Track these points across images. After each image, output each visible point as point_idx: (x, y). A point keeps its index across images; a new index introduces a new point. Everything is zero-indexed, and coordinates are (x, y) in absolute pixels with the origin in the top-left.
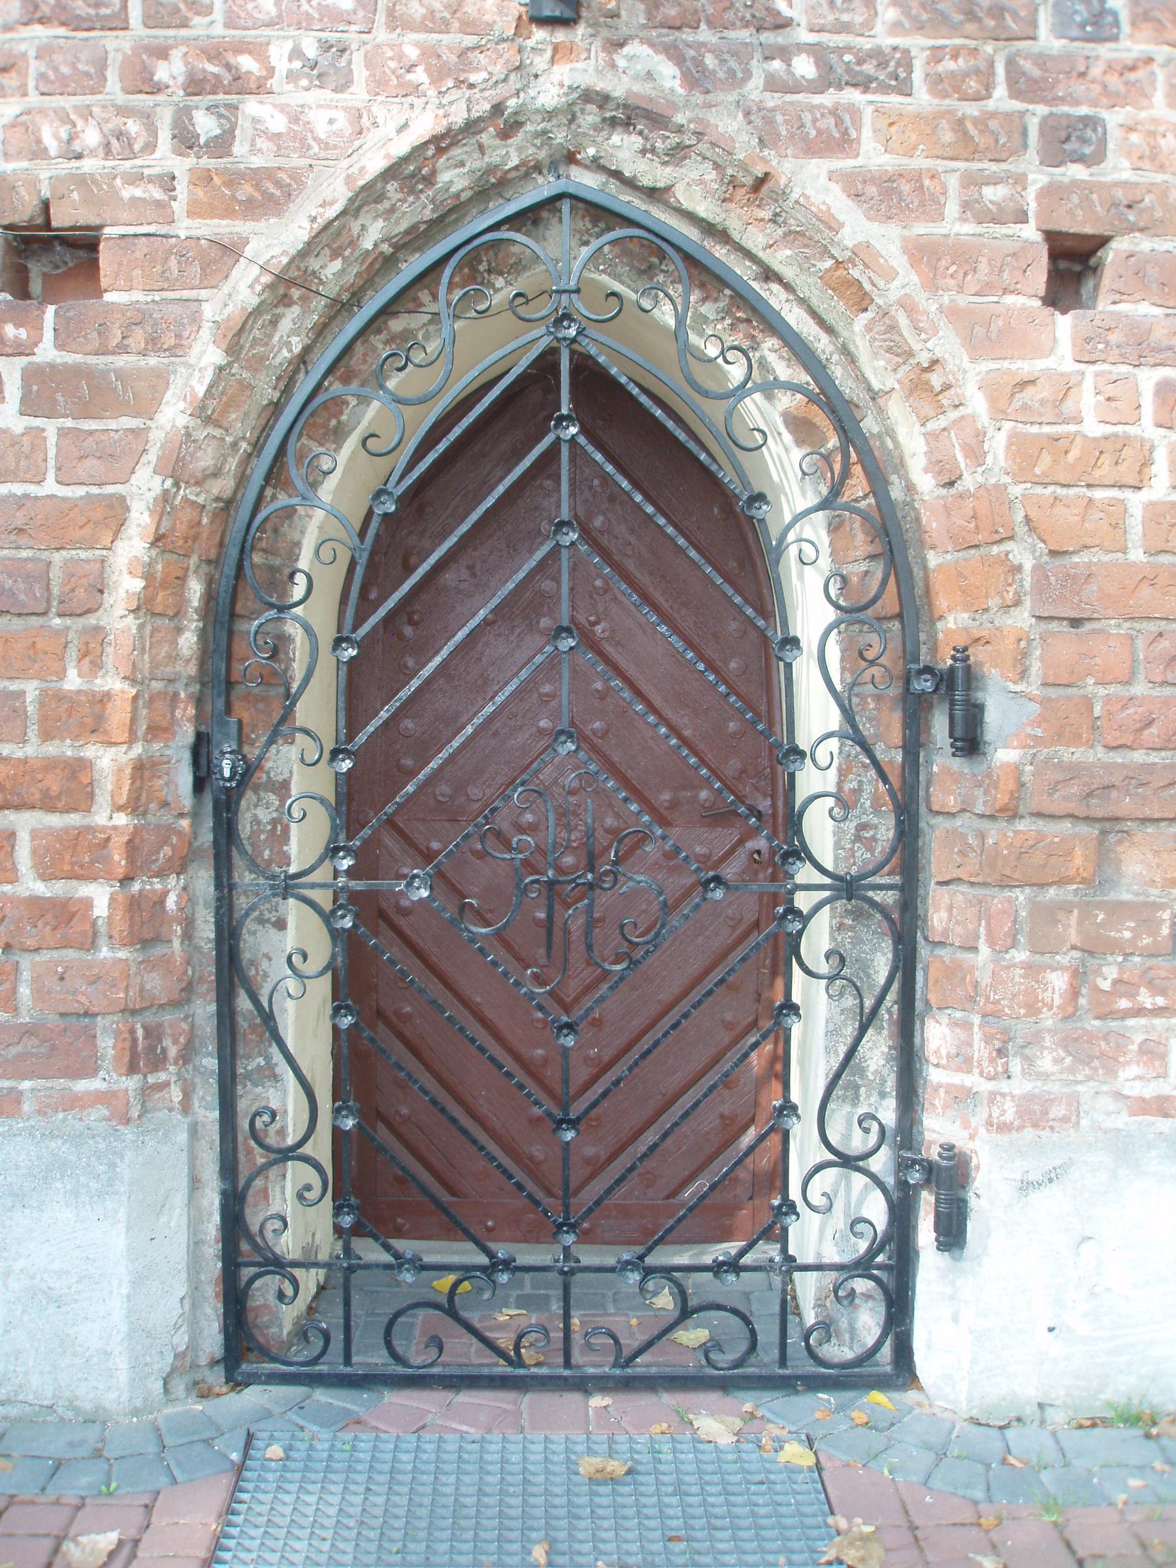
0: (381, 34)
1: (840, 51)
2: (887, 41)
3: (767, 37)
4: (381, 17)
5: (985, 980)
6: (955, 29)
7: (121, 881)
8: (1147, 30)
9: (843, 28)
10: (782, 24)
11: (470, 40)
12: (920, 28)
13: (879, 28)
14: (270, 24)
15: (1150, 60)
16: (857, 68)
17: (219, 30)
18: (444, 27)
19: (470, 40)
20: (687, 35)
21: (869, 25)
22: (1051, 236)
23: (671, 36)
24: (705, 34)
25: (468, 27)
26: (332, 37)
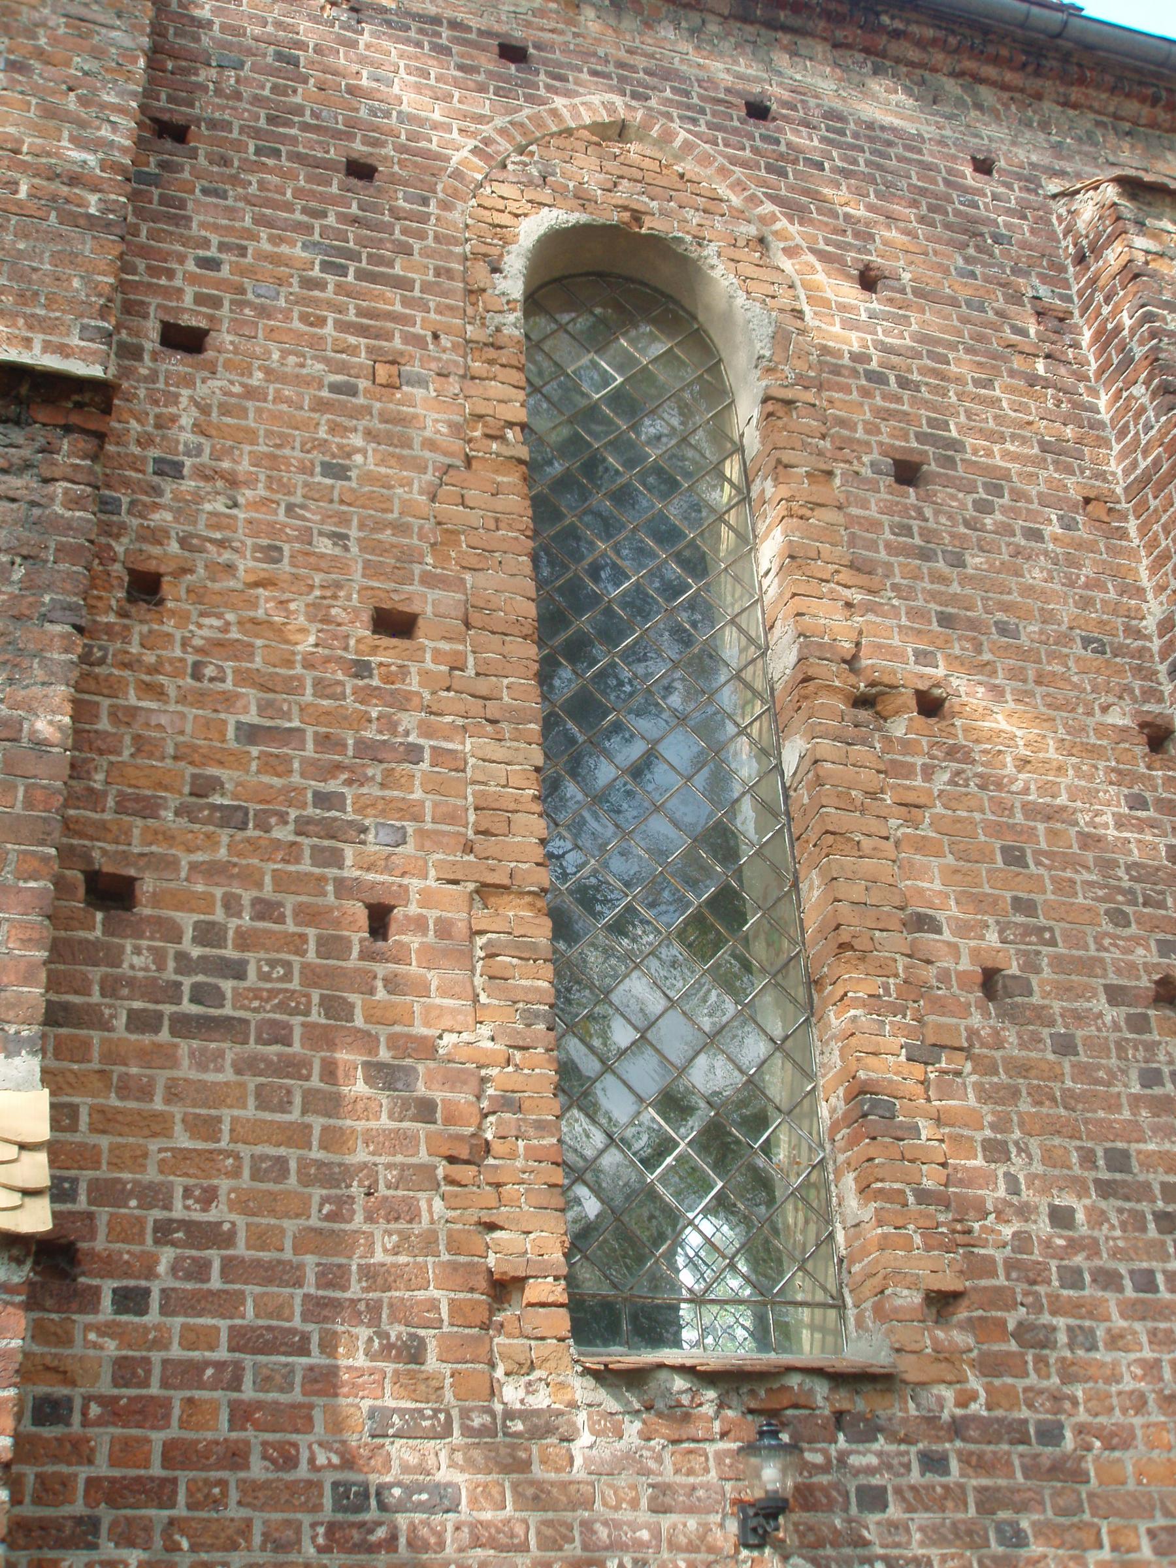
0: (665, 1555)
1: (897, 1558)
2: (921, 1552)
3: (859, 1551)
4: (664, 1545)
5: (606, 1291)
6: (950, 1544)
7: (594, 798)
8: (1042, 1540)
9: (897, 1545)
10: (866, 1544)
11: (712, 1557)
12: (934, 1543)
13: (914, 1544)
14: (607, 1548)
15: (1045, 1556)
16: (680, 1261)
17: (579, 1552)
18: (697, 1550)
19: (712, 1557)
20: (821, 1552)
21: (909, 1543)
22: (131, 572)
23: (812, 1553)
24: (829, 1551)
25: (711, 1550)
26: (639, 1555)
